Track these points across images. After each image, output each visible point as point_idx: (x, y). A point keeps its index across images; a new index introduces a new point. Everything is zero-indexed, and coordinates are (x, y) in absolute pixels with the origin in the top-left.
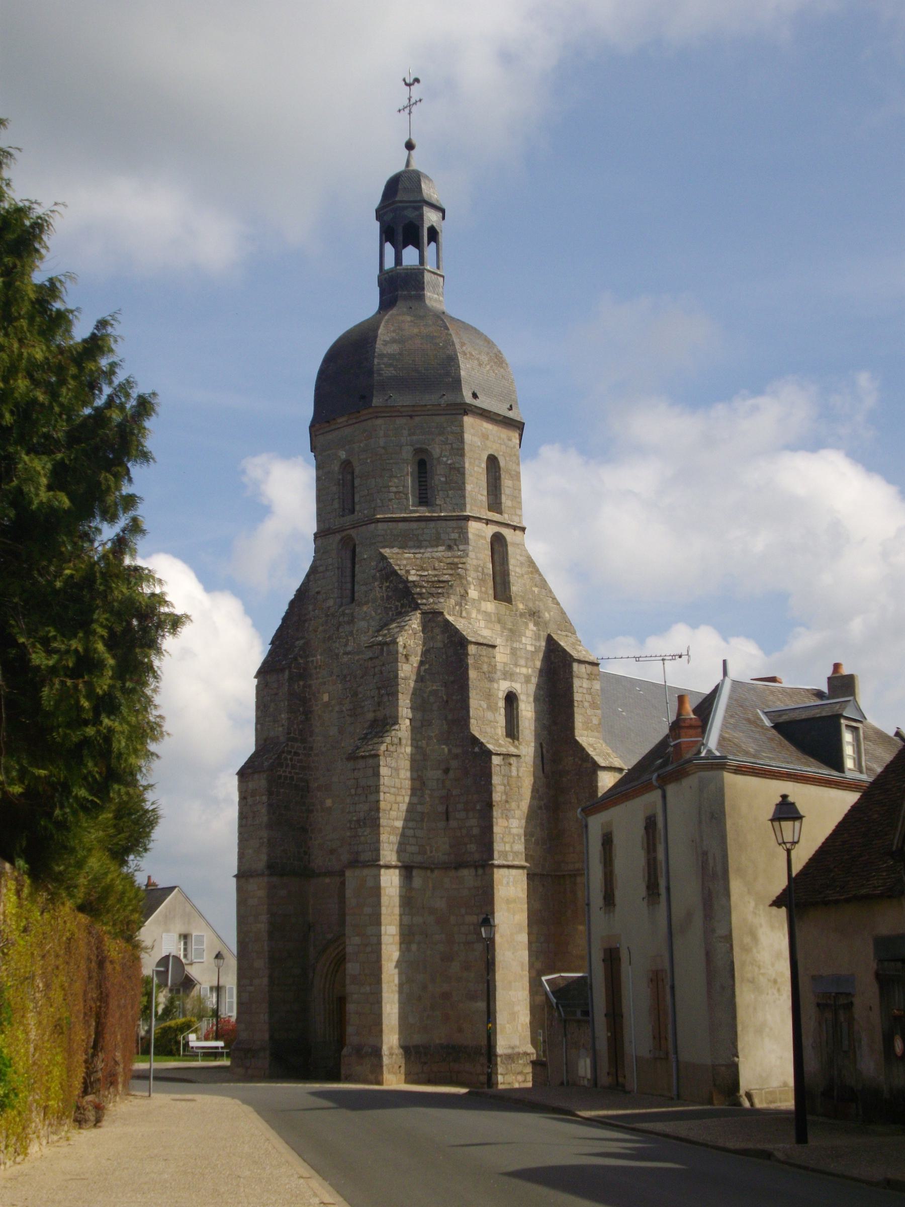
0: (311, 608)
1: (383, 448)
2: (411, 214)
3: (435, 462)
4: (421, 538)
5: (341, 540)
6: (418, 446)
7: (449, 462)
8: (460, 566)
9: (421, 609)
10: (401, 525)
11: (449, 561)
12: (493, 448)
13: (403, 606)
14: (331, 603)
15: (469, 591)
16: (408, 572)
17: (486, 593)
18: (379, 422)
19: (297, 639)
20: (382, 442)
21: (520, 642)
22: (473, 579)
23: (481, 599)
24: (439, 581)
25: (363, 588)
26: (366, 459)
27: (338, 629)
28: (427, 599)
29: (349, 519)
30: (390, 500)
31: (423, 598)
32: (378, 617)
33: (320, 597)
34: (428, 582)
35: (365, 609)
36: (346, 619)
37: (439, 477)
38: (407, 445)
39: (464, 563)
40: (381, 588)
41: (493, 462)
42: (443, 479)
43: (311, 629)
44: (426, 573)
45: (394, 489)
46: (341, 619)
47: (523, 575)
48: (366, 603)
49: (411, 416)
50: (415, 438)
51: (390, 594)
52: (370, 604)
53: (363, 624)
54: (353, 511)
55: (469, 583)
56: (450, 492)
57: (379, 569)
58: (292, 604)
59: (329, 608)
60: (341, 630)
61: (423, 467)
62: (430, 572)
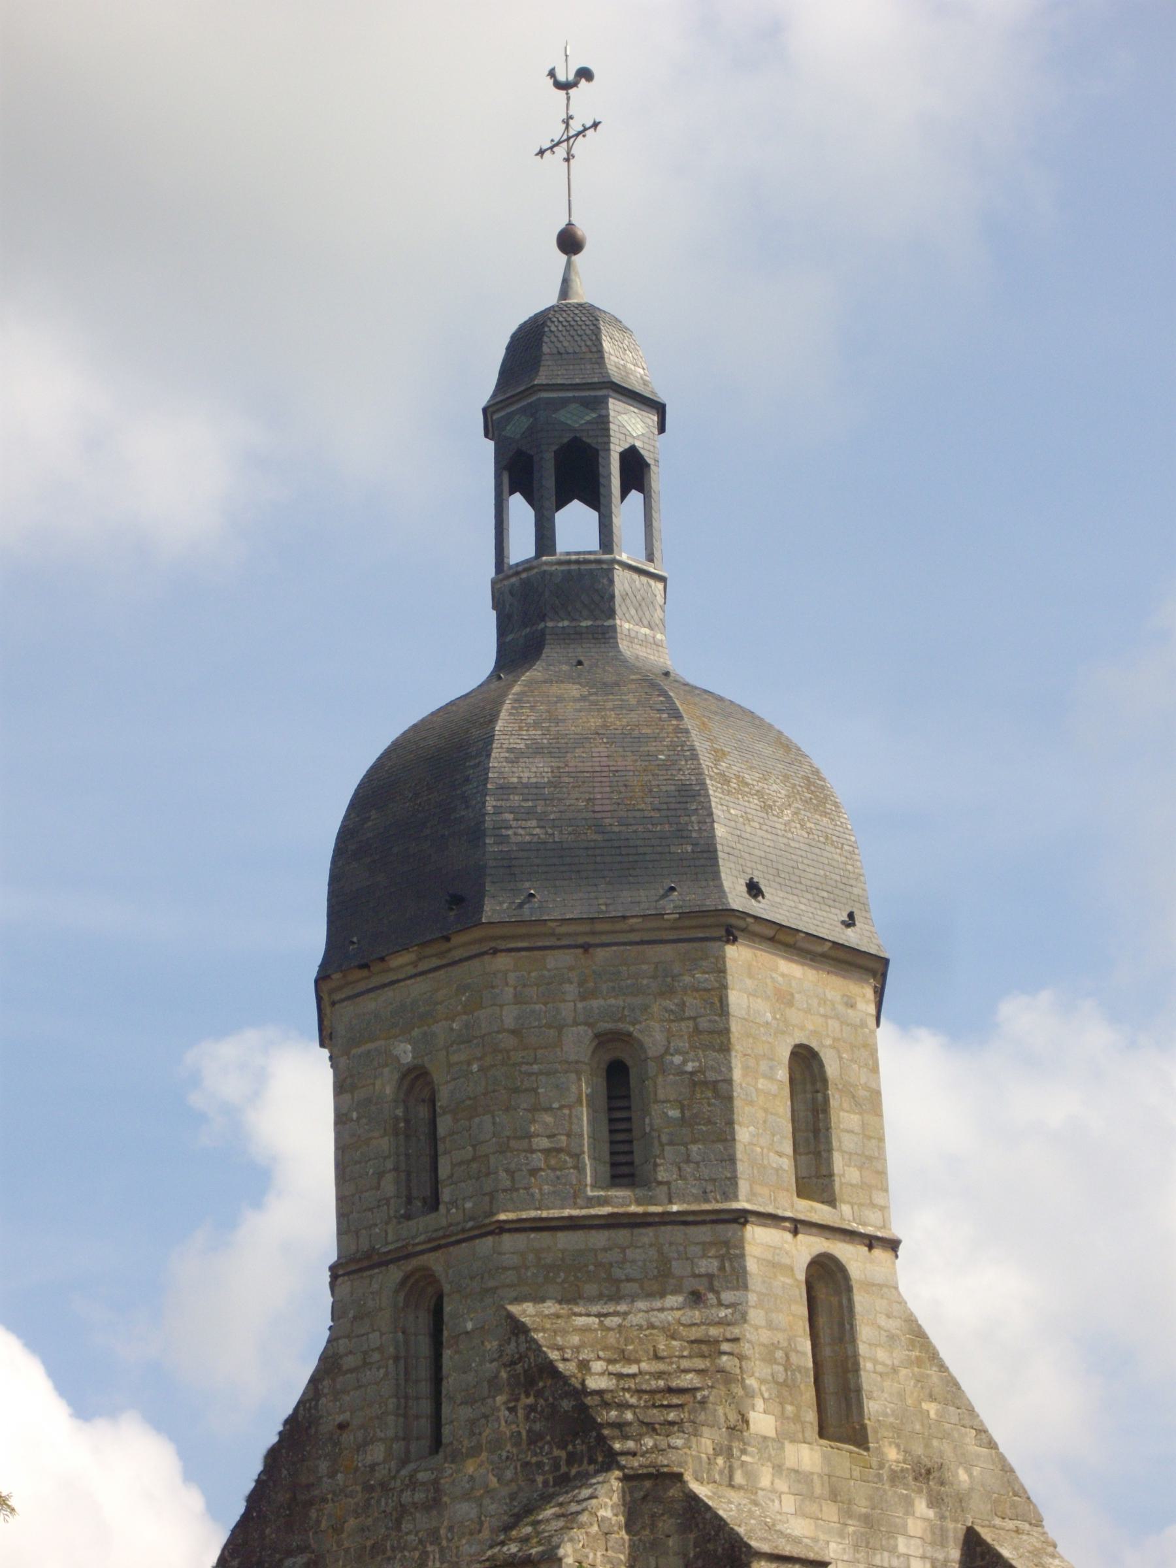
0: (323, 1467)
1: (513, 1032)
2: (575, 419)
3: (652, 1067)
4: (617, 1273)
5: (407, 1278)
6: (609, 1026)
7: (690, 1067)
8: (725, 1347)
9: (621, 1468)
10: (565, 1240)
11: (695, 1333)
12: (804, 1029)
13: (572, 1459)
14: (377, 1452)
15: (752, 1416)
16: (584, 1365)
17: (797, 1419)
18: (502, 962)
19: (290, 1553)
20: (510, 1015)
21: (893, 1550)
22: (762, 1381)
23: (782, 1437)
24: (670, 1390)
25: (466, 1412)
26: (469, 1064)
27: (398, 1522)
28: (638, 1439)
29: (423, 1225)
30: (534, 1172)
31: (626, 1437)
32: (505, 1491)
33: (347, 1438)
34: (639, 1392)
35: (470, 1467)
36: (419, 1496)
37: (663, 1108)
38: (576, 1023)
39: (736, 1340)
40: (512, 1410)
41: (806, 1064)
42: (674, 1113)
43: (324, 1525)
44: (633, 1369)
45: (545, 1143)
46: (406, 1497)
47: (895, 1370)
48: (475, 1451)
49: (586, 948)
50: (595, 1003)
51: (537, 1427)
52: (484, 1455)
53: (465, 1510)
54: (433, 1203)
55: (749, 1394)
56: (694, 1148)
57: (506, 1359)
58: (273, 1457)
59: (373, 1467)
60: (406, 1526)
61: (619, 1079)
62: (644, 1366)
